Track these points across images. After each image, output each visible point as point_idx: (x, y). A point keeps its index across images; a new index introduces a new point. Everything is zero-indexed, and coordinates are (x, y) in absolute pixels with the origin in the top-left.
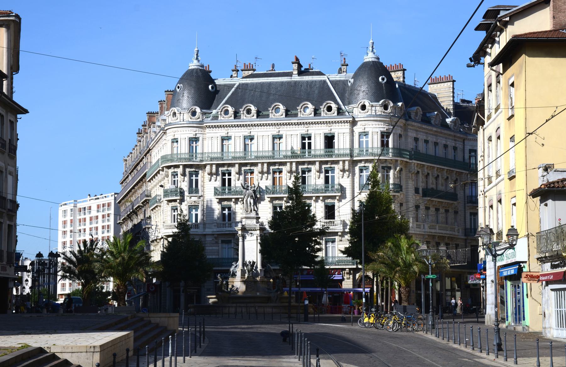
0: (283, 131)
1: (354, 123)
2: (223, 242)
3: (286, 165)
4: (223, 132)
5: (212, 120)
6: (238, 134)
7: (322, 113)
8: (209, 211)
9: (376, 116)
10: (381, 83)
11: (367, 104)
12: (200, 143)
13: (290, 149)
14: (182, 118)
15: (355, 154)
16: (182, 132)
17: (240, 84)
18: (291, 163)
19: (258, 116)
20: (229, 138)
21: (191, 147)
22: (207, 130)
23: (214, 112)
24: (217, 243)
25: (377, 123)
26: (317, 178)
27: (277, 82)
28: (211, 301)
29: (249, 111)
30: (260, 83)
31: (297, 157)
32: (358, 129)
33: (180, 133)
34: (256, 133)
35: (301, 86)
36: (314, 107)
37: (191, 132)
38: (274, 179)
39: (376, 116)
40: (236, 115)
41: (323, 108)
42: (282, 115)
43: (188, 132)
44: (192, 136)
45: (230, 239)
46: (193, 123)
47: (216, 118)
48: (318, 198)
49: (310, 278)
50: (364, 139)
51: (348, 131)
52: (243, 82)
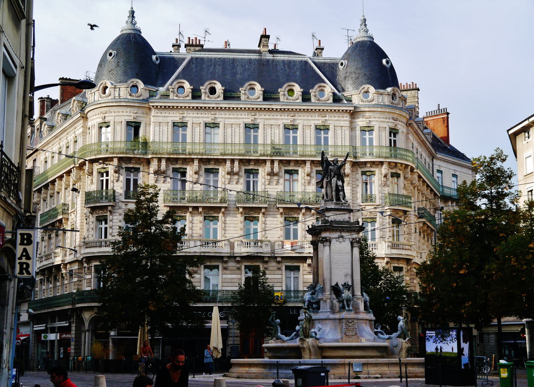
0: (261, 119)
1: (354, 114)
2: (288, 268)
3: (113, 161)
4: (176, 116)
5: (160, 98)
6: (307, 124)
7: (203, 95)
8: (358, 222)
9: (382, 106)
10: (384, 66)
11: (109, 85)
12: (331, 133)
13: (269, 142)
14: (117, 95)
15: (359, 155)
16: (117, 114)
17: (192, 58)
18: (272, 162)
19: (226, 98)
20: (216, 125)
21: (175, 135)
22: (153, 112)
23: (162, 90)
24: (239, 269)
25: (129, 109)
26: (307, 184)
27: (242, 59)
28: (183, 357)
29: (213, 91)
30: (220, 59)
31: (279, 153)
32: (361, 122)
33: (113, 114)
34: (262, 121)
35: (277, 65)
36: (302, 90)
37: (129, 115)
38: (248, 183)
39: (382, 106)
40: (196, 95)
41: (204, 89)
42: (259, 98)
43: (125, 114)
44: (131, 119)
45: (401, 265)
46: (133, 101)
47: (166, 96)
48: (196, 208)
49: (62, 325)
50: (367, 136)
51: (347, 124)
52: (197, 56)
